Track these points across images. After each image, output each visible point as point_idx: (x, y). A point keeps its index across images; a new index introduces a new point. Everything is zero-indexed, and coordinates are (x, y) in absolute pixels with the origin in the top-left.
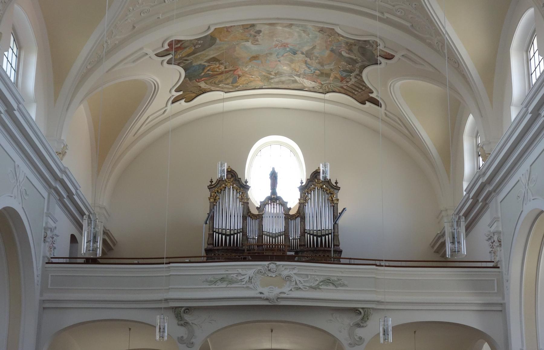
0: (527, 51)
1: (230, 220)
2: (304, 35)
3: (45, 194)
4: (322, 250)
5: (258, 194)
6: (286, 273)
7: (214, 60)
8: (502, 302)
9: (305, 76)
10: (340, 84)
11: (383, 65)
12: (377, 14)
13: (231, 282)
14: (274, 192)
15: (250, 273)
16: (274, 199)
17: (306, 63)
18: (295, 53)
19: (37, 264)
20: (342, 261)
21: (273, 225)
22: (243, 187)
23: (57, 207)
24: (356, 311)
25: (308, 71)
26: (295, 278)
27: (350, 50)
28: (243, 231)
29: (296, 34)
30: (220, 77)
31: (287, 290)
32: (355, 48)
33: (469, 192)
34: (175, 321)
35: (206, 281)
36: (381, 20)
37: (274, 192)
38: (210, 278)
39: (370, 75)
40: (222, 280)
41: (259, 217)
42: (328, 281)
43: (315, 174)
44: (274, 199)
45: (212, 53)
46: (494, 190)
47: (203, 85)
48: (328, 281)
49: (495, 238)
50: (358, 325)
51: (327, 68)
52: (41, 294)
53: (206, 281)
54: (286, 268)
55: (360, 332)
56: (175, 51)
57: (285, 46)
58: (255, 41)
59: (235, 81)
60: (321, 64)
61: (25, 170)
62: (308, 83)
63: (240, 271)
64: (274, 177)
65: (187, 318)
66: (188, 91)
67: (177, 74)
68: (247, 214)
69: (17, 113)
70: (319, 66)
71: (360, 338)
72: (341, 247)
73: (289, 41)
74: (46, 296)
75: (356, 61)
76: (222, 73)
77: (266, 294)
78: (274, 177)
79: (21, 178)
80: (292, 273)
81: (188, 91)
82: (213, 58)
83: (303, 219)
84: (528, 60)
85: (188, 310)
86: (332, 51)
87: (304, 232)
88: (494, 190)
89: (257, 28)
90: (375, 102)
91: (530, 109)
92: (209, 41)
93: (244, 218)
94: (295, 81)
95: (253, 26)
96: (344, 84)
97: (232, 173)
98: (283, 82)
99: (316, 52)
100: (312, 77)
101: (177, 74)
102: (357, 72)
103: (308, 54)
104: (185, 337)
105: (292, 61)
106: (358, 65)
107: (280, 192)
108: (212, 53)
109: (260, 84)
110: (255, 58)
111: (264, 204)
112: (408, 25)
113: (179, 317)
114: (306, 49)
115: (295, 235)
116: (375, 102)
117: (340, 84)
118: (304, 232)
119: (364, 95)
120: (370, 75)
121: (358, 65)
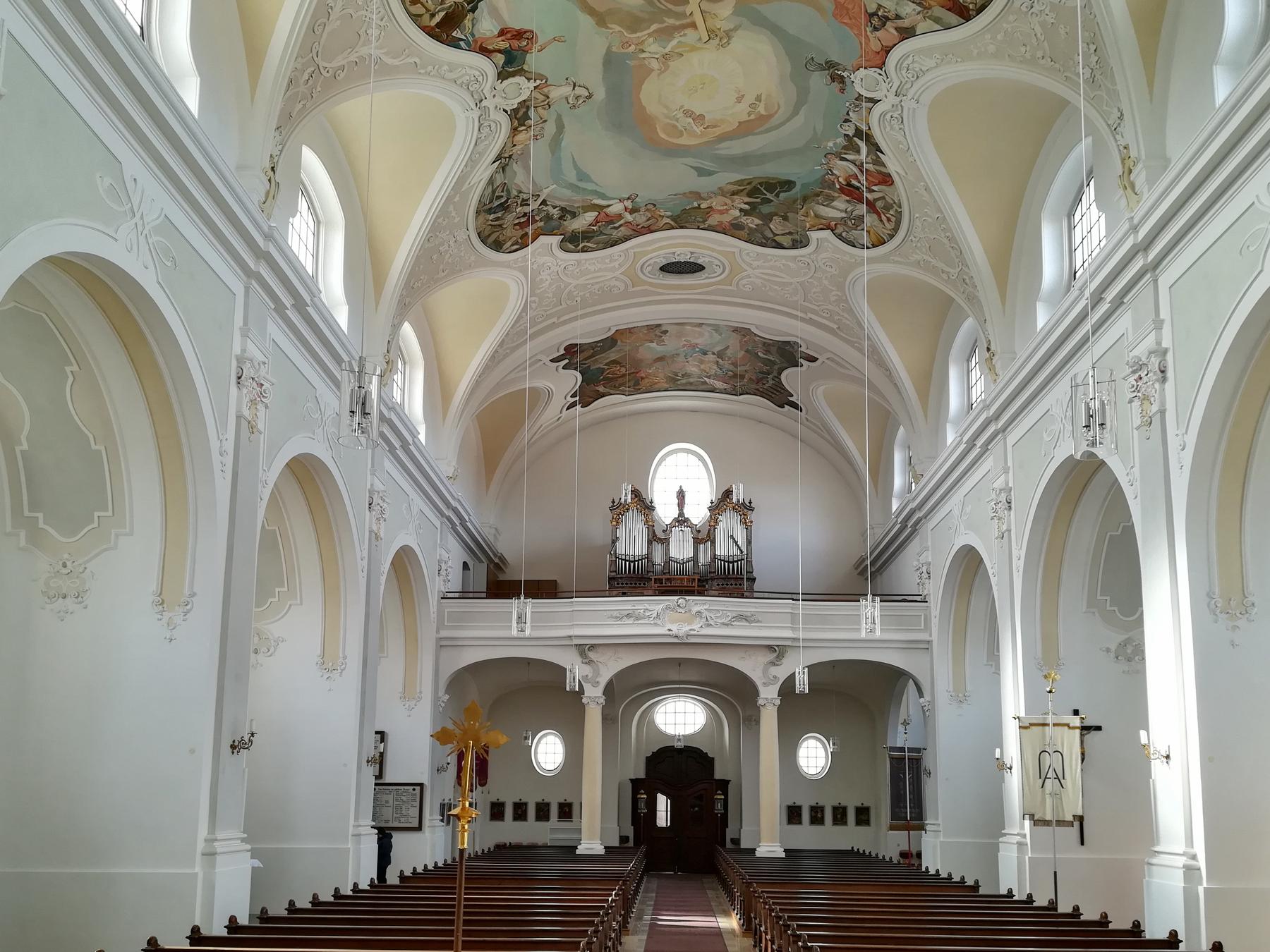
0: (969, 360)
1: (632, 541)
2: (715, 334)
3: (438, 524)
4: (731, 580)
5: (666, 511)
6: (695, 609)
7: (615, 362)
8: (928, 638)
9: (716, 377)
10: (755, 386)
11: (804, 368)
12: (799, 314)
13: (638, 618)
14: (681, 514)
15: (659, 608)
16: (681, 520)
17: (717, 363)
18: (705, 354)
19: (433, 599)
20: (756, 595)
21: (681, 549)
22: (646, 507)
23: (450, 536)
24: (770, 648)
25: (719, 372)
26: (705, 614)
27: (767, 352)
28: (648, 557)
29: (707, 334)
30: (620, 381)
31: (696, 627)
32: (774, 349)
33: (897, 517)
34: (579, 660)
35: (612, 617)
36: (803, 320)
37: (681, 514)
38: (615, 614)
39: (791, 378)
40: (629, 616)
41: (666, 542)
42: (741, 617)
43: (728, 493)
44: (681, 520)
45: (613, 355)
46: (925, 516)
47: (601, 389)
48: (741, 617)
49: (924, 569)
50: (773, 664)
51: (740, 369)
52: (438, 632)
53: (612, 617)
54: (698, 604)
55: (774, 671)
56: (571, 355)
57: (694, 346)
58: (661, 342)
59: (637, 384)
60: (735, 364)
61: (418, 502)
62: (719, 384)
63: (647, 606)
64: (681, 495)
65: (592, 655)
66: (586, 396)
67: (573, 379)
68: (653, 538)
69: (412, 447)
70: (732, 368)
71: (775, 677)
72: (755, 574)
73: (699, 341)
74: (444, 633)
75: (774, 363)
76: (624, 375)
77: (675, 631)
78: (681, 495)
79: (415, 511)
80: (701, 608)
81: (586, 396)
82: (563, 127)
83: (713, 543)
84: (969, 371)
85: (593, 647)
86: (747, 351)
87: (714, 558)
88: (925, 516)
89: (664, 328)
90: (795, 406)
91: (965, 439)
92: (610, 342)
93: (650, 543)
94: (705, 383)
95: (659, 325)
96: (760, 386)
97: (636, 493)
98: (691, 384)
99: (729, 352)
100: (723, 378)
101: (573, 379)
102: (775, 374)
103: (720, 355)
104: (590, 675)
105: (702, 362)
106: (776, 367)
107: (688, 512)
108: (613, 355)
109: (666, 386)
110: (661, 359)
111: (671, 526)
112: (835, 327)
113: (583, 654)
114: (717, 349)
115: (704, 558)
116: (795, 406)
117: (755, 386)
118: (714, 558)
119: (781, 397)
120: (791, 378)
121: (776, 367)
